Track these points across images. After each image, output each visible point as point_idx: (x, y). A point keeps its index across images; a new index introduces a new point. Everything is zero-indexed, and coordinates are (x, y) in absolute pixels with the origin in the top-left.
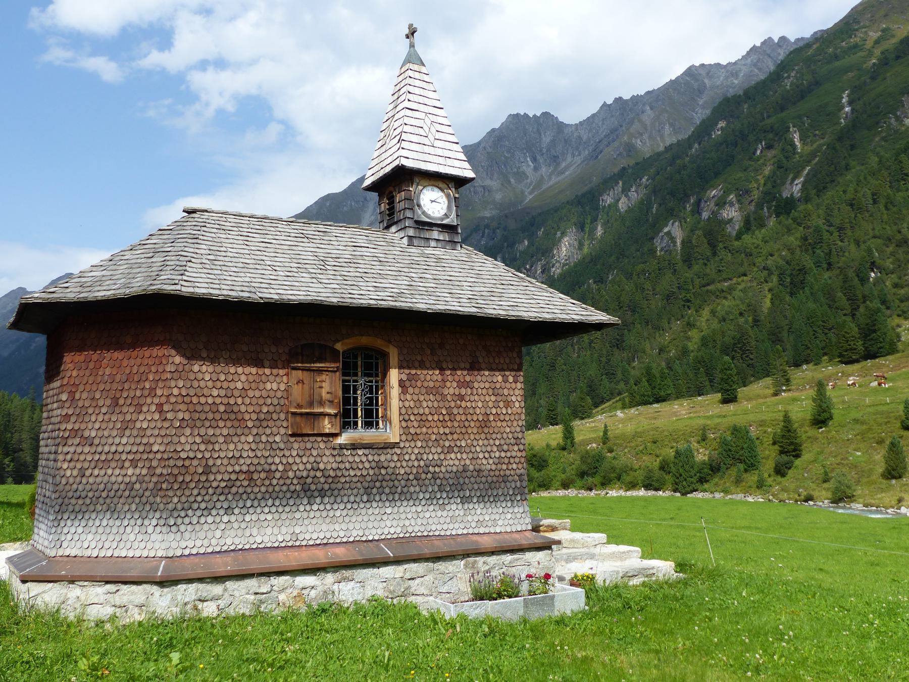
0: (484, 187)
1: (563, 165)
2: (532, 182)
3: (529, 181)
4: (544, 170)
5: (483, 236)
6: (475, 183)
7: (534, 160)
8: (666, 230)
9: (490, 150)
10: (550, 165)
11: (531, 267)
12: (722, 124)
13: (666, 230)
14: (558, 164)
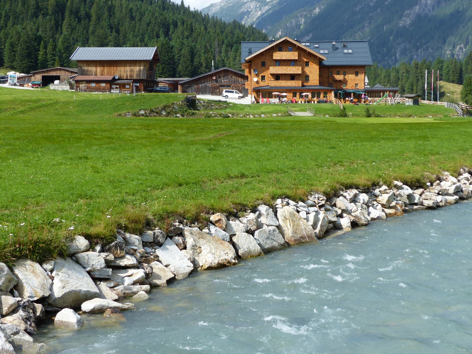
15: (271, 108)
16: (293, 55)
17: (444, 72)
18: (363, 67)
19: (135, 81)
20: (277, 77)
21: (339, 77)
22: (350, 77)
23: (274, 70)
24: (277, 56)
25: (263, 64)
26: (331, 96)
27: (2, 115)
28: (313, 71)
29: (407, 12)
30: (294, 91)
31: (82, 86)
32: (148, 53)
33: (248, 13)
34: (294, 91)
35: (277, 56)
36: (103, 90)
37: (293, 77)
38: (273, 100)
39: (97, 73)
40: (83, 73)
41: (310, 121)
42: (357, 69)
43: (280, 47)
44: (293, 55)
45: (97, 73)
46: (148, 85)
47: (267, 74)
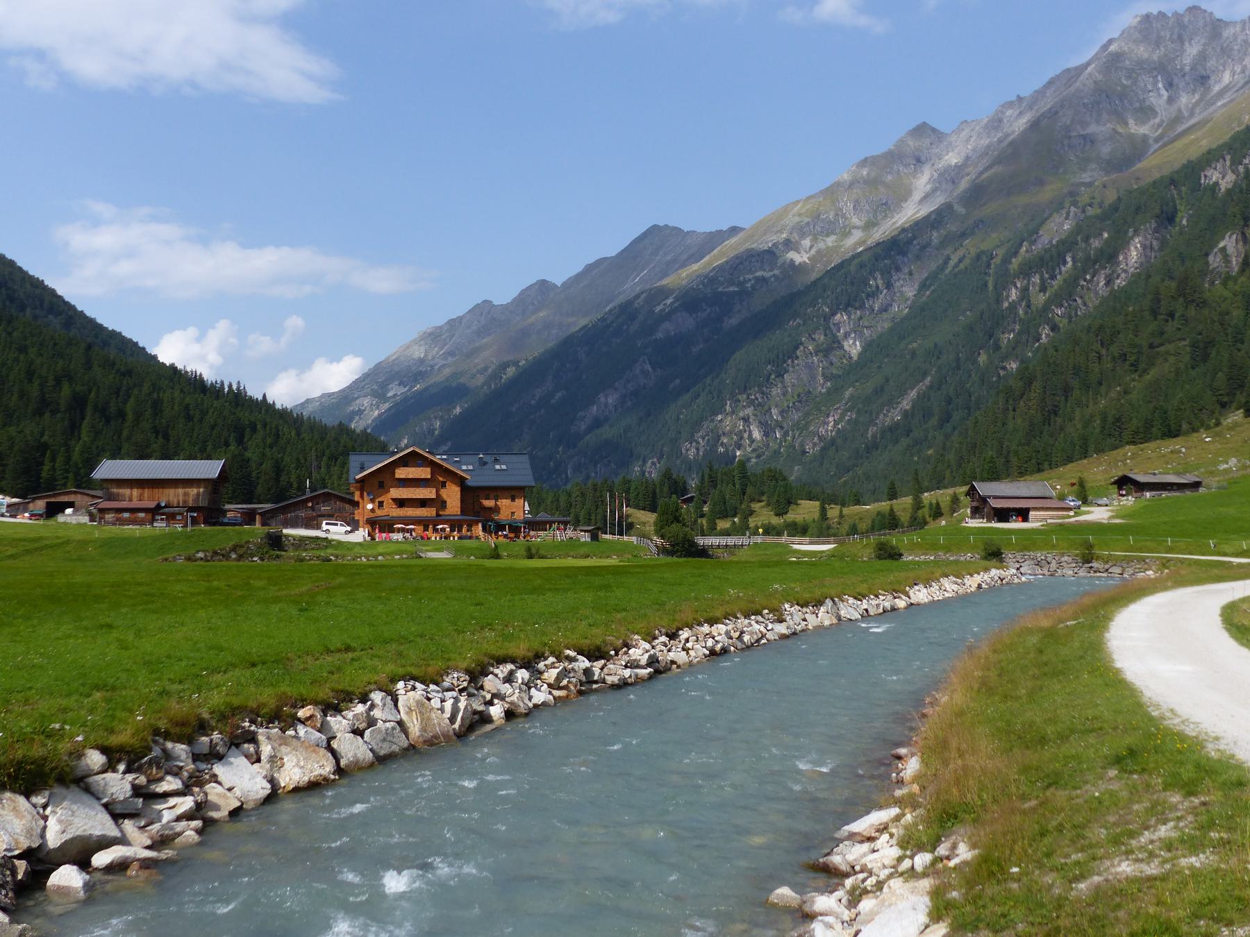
0: (1084, 137)
1: (1217, 88)
2: (1162, 121)
3: (1157, 120)
4: (1184, 100)
5: (1067, 218)
6: (100, 736)
7: (1170, 85)
8: (1221, 245)
9: (1100, 77)
10: (1194, 91)
11: (1093, 276)
12: (678, 381)
13: (1221, 245)
14: (1208, 89)
19: (191, 509)
20: (401, 503)
21: (489, 503)
22: (504, 503)
23: (396, 493)
24: (401, 473)
26: (478, 530)
28: (452, 495)
29: (581, 413)
30: (425, 523)
32: (211, 468)
35: (401, 473)
36: (141, 523)
37: (423, 503)
39: (133, 497)
40: (111, 497)
42: (513, 492)
43: (405, 461)
45: (133, 497)
46: (211, 514)
47: (386, 498)
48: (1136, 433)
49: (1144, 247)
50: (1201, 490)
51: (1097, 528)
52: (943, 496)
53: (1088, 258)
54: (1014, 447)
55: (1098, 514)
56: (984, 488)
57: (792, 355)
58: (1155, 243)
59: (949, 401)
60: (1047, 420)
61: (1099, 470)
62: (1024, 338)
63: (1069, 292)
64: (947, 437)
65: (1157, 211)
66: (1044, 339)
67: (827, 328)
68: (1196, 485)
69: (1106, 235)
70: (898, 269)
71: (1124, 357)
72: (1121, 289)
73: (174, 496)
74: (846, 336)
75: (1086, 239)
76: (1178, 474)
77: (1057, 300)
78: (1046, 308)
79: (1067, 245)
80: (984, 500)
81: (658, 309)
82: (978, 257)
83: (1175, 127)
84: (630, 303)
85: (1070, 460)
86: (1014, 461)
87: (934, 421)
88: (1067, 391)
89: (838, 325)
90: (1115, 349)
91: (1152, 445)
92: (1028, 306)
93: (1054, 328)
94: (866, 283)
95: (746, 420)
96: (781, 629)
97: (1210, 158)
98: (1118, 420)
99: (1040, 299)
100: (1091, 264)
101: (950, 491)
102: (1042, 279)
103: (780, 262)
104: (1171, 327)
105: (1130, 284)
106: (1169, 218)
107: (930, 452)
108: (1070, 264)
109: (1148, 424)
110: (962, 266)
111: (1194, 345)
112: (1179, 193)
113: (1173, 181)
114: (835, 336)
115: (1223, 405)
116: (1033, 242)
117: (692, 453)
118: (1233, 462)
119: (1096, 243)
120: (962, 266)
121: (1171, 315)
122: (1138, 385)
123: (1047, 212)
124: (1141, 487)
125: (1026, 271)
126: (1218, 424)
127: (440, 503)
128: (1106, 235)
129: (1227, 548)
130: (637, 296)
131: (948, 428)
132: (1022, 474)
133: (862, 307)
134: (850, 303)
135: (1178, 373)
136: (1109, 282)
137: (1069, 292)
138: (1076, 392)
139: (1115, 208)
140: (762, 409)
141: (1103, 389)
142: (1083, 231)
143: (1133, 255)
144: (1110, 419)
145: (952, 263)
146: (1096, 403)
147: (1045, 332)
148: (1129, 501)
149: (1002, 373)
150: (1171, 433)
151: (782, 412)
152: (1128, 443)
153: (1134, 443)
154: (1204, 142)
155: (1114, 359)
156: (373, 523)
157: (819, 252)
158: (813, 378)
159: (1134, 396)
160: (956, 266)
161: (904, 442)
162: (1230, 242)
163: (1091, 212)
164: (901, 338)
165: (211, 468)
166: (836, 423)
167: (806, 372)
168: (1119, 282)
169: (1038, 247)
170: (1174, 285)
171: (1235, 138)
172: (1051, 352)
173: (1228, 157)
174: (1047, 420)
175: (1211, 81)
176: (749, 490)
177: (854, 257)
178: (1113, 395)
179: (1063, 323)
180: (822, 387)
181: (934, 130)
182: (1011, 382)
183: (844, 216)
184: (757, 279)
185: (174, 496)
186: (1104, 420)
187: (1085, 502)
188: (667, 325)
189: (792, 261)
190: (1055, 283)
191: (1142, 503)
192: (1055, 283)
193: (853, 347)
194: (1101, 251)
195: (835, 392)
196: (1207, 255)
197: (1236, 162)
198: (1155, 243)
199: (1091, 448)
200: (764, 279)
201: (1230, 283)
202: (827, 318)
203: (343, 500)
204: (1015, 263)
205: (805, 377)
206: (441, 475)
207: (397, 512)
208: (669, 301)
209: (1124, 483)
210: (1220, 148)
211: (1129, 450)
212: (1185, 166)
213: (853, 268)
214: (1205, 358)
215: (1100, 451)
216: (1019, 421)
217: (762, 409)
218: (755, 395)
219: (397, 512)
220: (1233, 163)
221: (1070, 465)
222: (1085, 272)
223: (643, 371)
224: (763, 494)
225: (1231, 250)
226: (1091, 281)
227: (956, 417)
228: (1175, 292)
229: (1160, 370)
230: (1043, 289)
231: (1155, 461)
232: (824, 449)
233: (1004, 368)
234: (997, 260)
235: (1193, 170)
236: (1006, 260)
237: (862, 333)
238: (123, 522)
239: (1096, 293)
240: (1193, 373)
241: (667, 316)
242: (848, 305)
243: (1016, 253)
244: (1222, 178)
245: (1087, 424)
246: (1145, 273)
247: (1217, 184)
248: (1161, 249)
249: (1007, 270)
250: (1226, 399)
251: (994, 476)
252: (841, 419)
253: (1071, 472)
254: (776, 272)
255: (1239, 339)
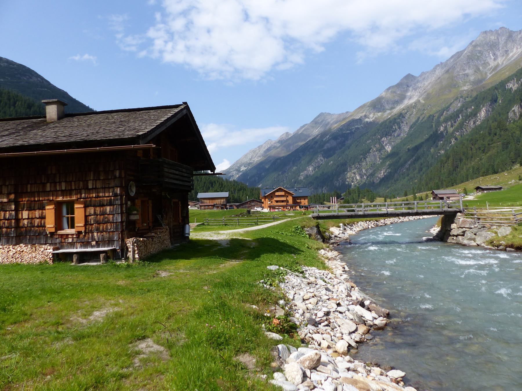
8: (513, 109)
13: (513, 109)
14: (508, 55)
15: (274, 213)
16: (283, 193)
17: (325, 198)
18: (307, 197)
19: (222, 205)
20: (277, 201)
21: (298, 201)
22: (302, 201)
23: (276, 199)
24: (277, 194)
25: (272, 197)
26: (298, 208)
27: (521, 203)
28: (290, 199)
29: (302, 173)
30: (283, 207)
31: (202, 207)
32: (226, 194)
33: (233, 176)
34: (284, 206)
35: (277, 194)
36: (211, 209)
37: (283, 201)
38: (276, 210)
39: (207, 202)
40: (202, 203)
41: (509, 206)
42: (305, 198)
43: (277, 191)
44: (283, 193)
45: (207, 202)
46: (224, 206)
47: (273, 201)
48: (484, 173)
49: (486, 111)
50: (502, 190)
51: (470, 201)
52: (423, 194)
53: (467, 116)
54: (444, 179)
55: (470, 198)
56: (436, 192)
57: (368, 152)
58: (490, 109)
59: (421, 164)
60: (454, 170)
61: (471, 185)
62: (446, 143)
63: (461, 126)
64: (421, 176)
65: (490, 98)
66: (453, 143)
67: (380, 143)
68: (500, 188)
69: (473, 107)
70: (402, 122)
71: (480, 148)
72: (479, 126)
73: (217, 202)
74: (386, 145)
75: (466, 109)
76: (495, 185)
77: (457, 130)
78: (453, 133)
79: (460, 111)
80: (436, 195)
81: (324, 139)
82: (429, 117)
83: (498, 64)
84: (315, 138)
85: (462, 182)
86: (444, 183)
87: (417, 171)
88: (461, 160)
89: (383, 142)
90: (476, 146)
91: (489, 176)
92: (447, 132)
93: (456, 139)
94: (392, 128)
95: (354, 173)
96: (400, 220)
97: (509, 79)
98: (478, 169)
99: (451, 130)
100: (468, 117)
101: (425, 193)
102: (451, 123)
103: (363, 122)
104: (495, 138)
105: (482, 123)
106: (494, 100)
107: (416, 181)
108: (461, 118)
109: (488, 170)
110: (424, 120)
111: (503, 144)
112: (498, 92)
113: (496, 88)
114: (382, 145)
115: (513, 162)
116: (448, 111)
117: (337, 184)
118: (513, 181)
119: (469, 110)
120: (424, 120)
121: (496, 134)
122: (485, 157)
123: (452, 100)
124: (483, 190)
125: (446, 121)
126: (511, 169)
127: (287, 201)
128: (473, 107)
129: (505, 205)
130: (317, 136)
131: (422, 173)
132: (447, 187)
133: (391, 135)
134: (387, 134)
135: (498, 152)
136: (474, 123)
137: (461, 126)
138: (464, 160)
139: (476, 98)
140: (360, 169)
141: (473, 159)
142: (465, 106)
143: (483, 114)
144: (475, 168)
145: (420, 119)
146: (471, 164)
147: (453, 141)
148: (480, 194)
149: (439, 154)
150: (495, 172)
151: (366, 170)
152: (481, 176)
153: (483, 176)
154: (507, 73)
155: (476, 149)
156: (270, 207)
157: (376, 118)
158: (376, 159)
159: (483, 161)
160: (422, 120)
161: (407, 178)
162: (516, 108)
163: (467, 100)
164: (404, 145)
165: (226, 194)
166: (384, 173)
167: (374, 157)
168: (478, 123)
169: (450, 113)
170: (496, 123)
171: (517, 72)
172: (455, 148)
173: (515, 79)
174: (454, 170)
175: (509, 52)
176: (360, 195)
177: (387, 120)
178: (476, 161)
179: (459, 137)
180: (379, 161)
181: (413, 76)
182: (442, 158)
183: (384, 106)
184: (356, 128)
185: (217, 202)
186: (473, 168)
187: (466, 194)
188: (327, 144)
189: (367, 122)
190: (456, 124)
191: (483, 194)
192: (456, 124)
193: (389, 148)
194: (471, 113)
195: (383, 163)
196: (508, 113)
197: (518, 80)
198: (490, 109)
199: (469, 177)
200: (358, 128)
201: (516, 123)
202: (379, 140)
203: (259, 202)
204: (442, 118)
205: (373, 159)
206: (287, 194)
207: (276, 204)
208: (328, 137)
209: (478, 188)
210: (512, 75)
211: (481, 178)
212: (500, 83)
213: (387, 123)
214: (507, 148)
215: (472, 179)
216: (445, 170)
217: (360, 169)
218: (357, 165)
219: (276, 204)
220: (517, 80)
221: (462, 184)
222: (466, 120)
223: (321, 160)
224: (365, 196)
225: (516, 110)
226: (468, 123)
227: (424, 169)
228: (496, 127)
229: (493, 152)
230: (452, 126)
231: (489, 181)
232: (380, 182)
233: (440, 153)
234: (436, 118)
235: (503, 84)
236: (439, 117)
237: (391, 144)
238: (205, 209)
239: (470, 127)
240: (503, 153)
241: (327, 142)
242: (386, 135)
243: (442, 115)
244: (513, 86)
245: (468, 170)
246: (487, 120)
247: (511, 88)
248: (492, 111)
249: (439, 120)
250: (514, 161)
251: (438, 188)
252: (385, 172)
253: (462, 186)
254: (362, 125)
255: (518, 141)
